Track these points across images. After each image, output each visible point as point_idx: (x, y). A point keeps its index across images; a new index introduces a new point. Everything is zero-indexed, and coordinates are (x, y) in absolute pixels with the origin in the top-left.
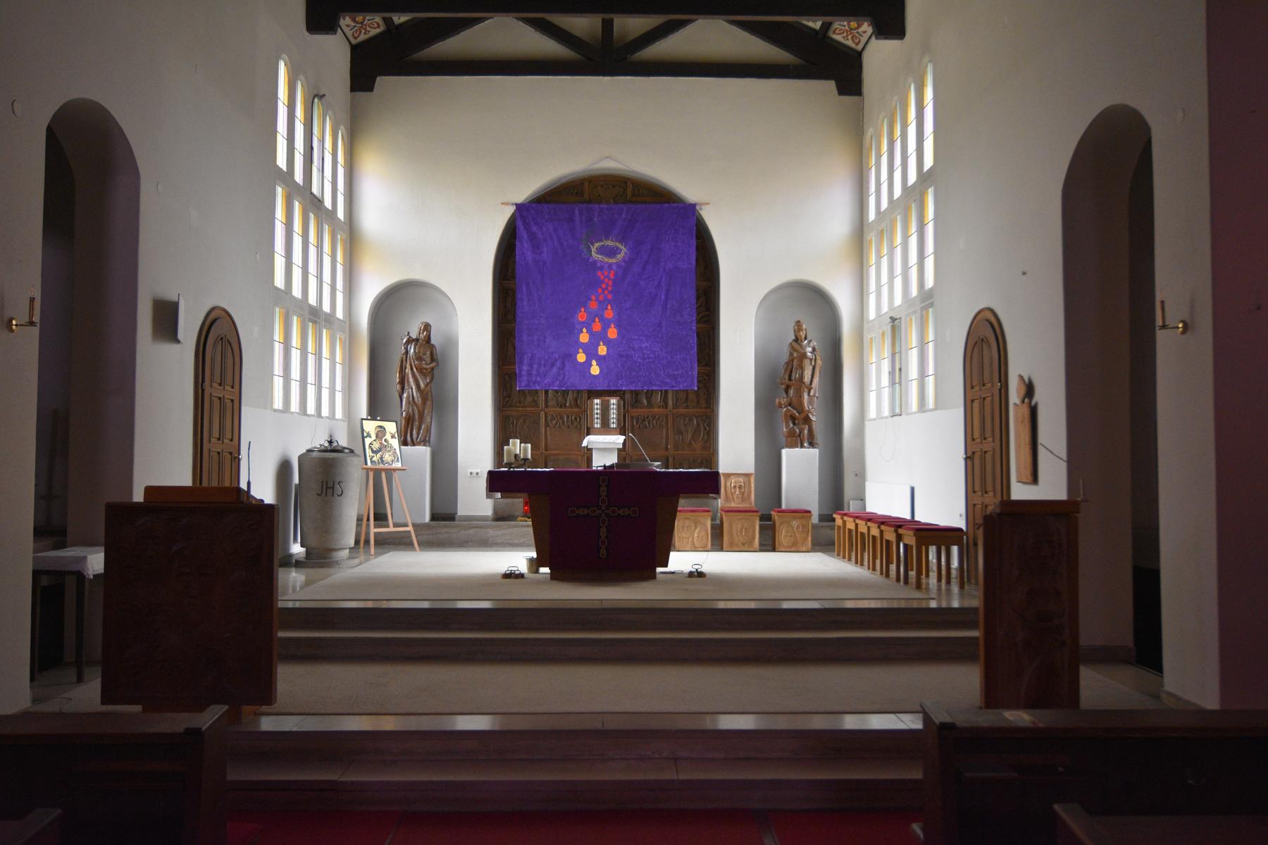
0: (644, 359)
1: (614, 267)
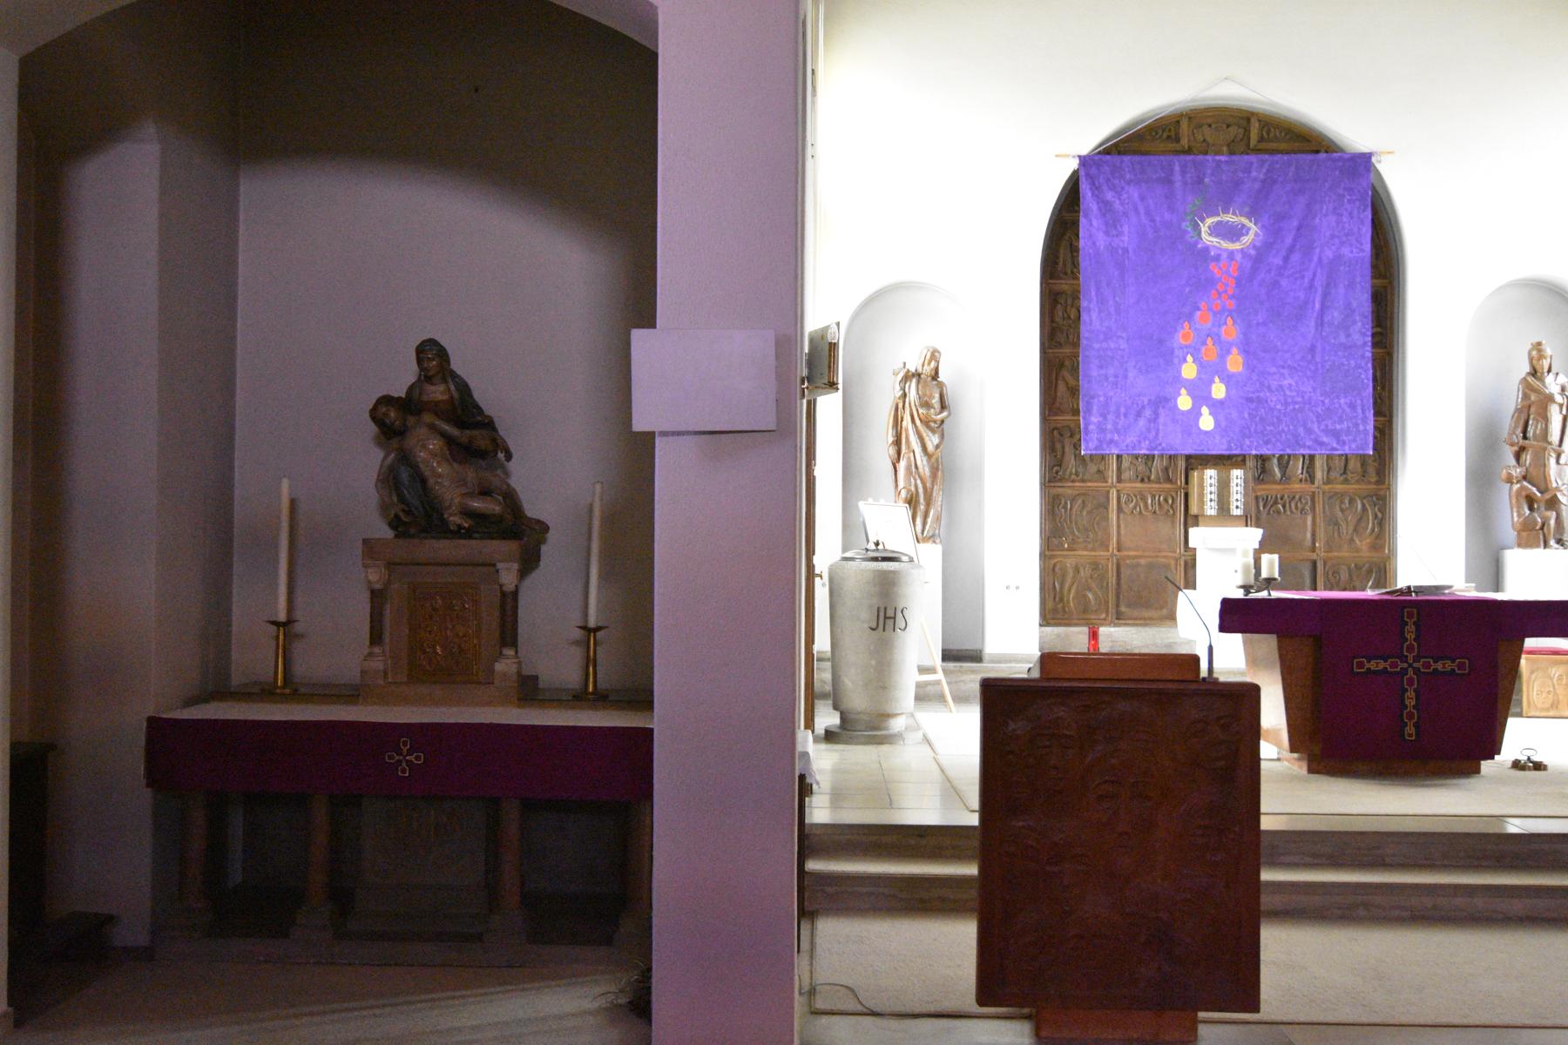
0: (1286, 404)
1: (1239, 257)
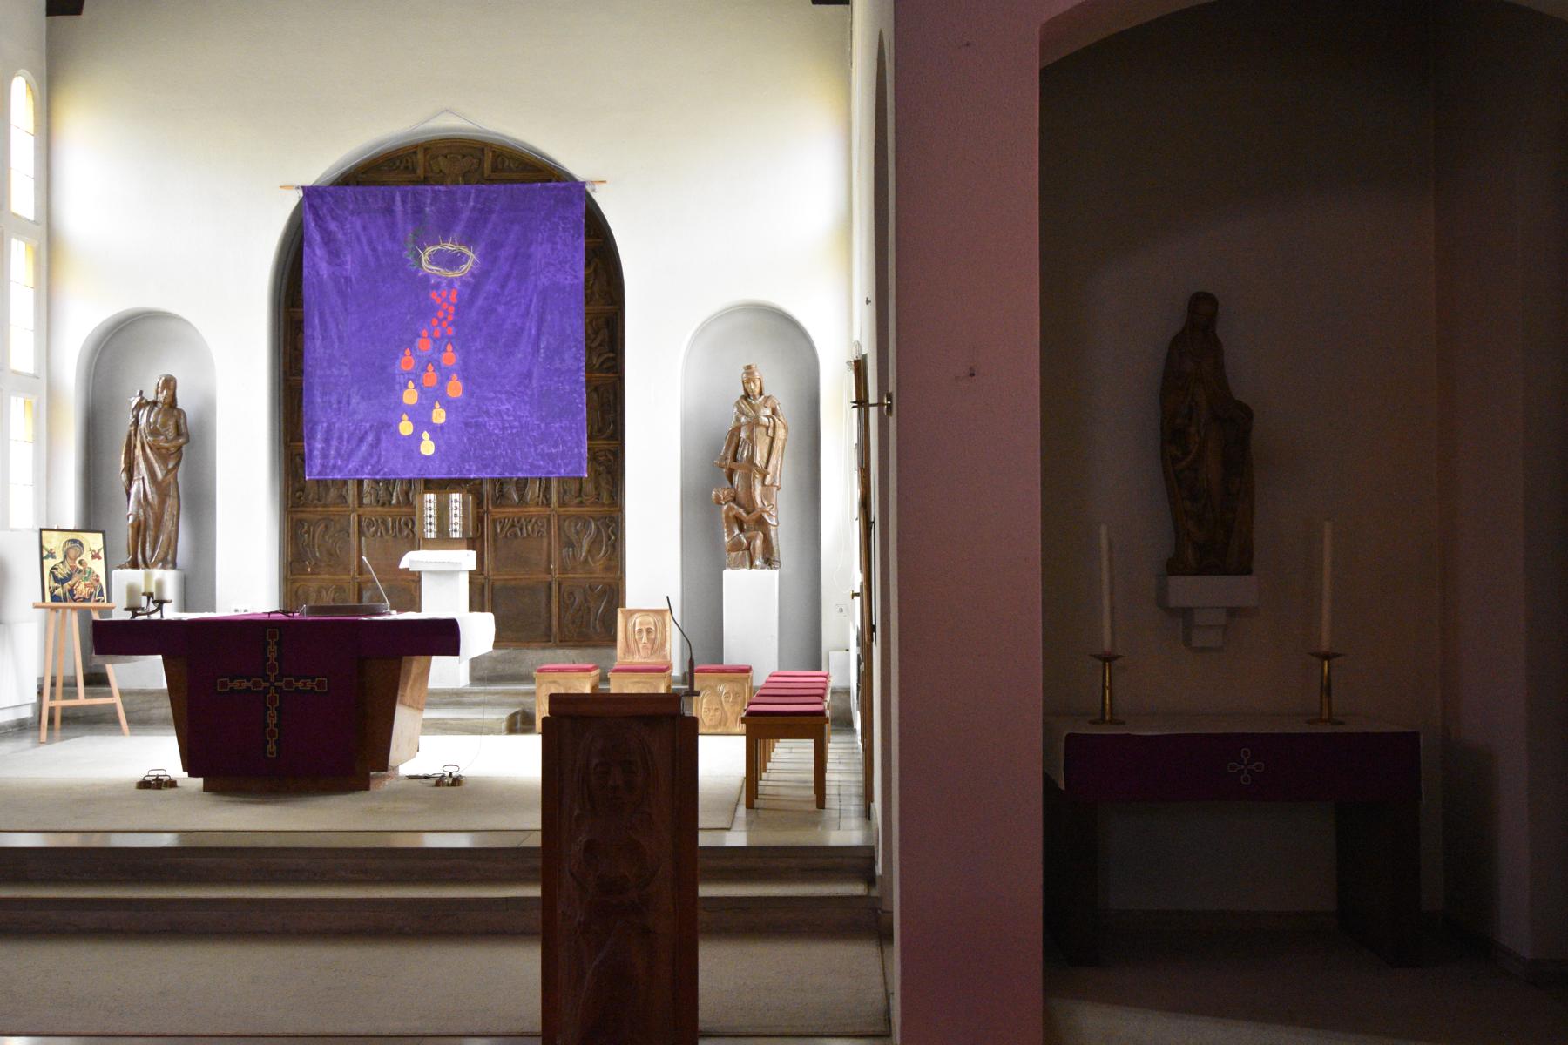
0: (503, 429)
1: (457, 285)
